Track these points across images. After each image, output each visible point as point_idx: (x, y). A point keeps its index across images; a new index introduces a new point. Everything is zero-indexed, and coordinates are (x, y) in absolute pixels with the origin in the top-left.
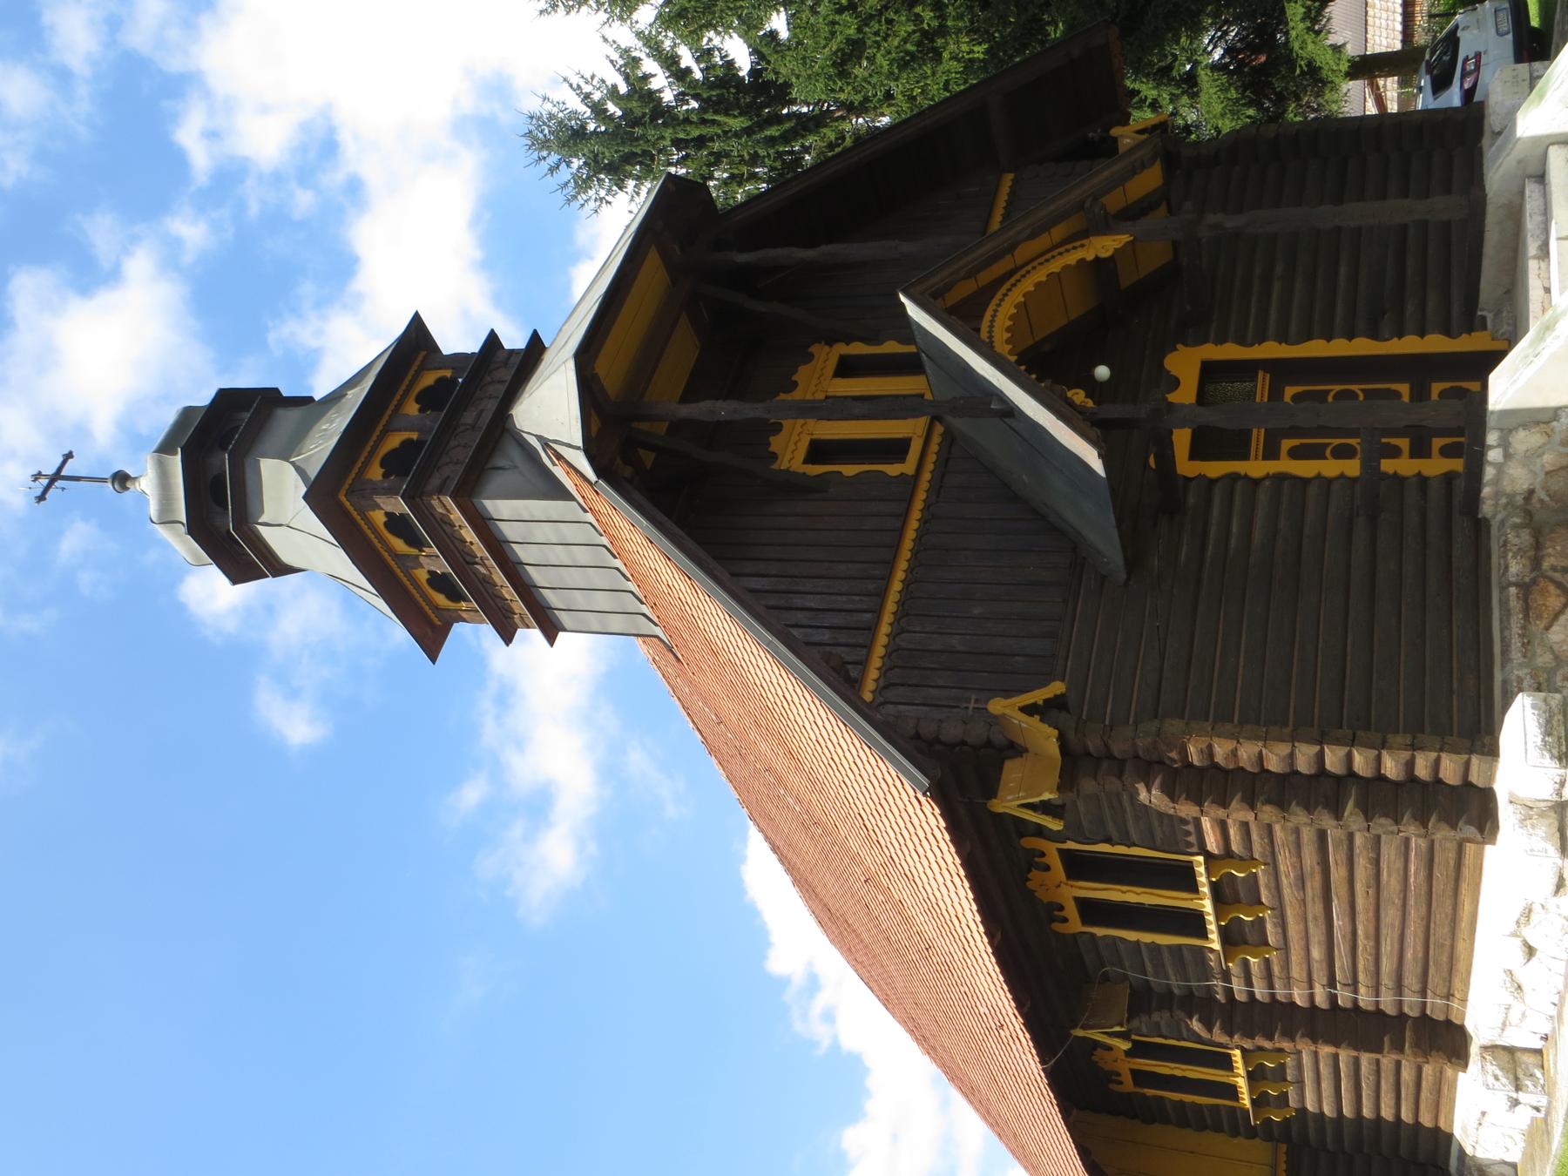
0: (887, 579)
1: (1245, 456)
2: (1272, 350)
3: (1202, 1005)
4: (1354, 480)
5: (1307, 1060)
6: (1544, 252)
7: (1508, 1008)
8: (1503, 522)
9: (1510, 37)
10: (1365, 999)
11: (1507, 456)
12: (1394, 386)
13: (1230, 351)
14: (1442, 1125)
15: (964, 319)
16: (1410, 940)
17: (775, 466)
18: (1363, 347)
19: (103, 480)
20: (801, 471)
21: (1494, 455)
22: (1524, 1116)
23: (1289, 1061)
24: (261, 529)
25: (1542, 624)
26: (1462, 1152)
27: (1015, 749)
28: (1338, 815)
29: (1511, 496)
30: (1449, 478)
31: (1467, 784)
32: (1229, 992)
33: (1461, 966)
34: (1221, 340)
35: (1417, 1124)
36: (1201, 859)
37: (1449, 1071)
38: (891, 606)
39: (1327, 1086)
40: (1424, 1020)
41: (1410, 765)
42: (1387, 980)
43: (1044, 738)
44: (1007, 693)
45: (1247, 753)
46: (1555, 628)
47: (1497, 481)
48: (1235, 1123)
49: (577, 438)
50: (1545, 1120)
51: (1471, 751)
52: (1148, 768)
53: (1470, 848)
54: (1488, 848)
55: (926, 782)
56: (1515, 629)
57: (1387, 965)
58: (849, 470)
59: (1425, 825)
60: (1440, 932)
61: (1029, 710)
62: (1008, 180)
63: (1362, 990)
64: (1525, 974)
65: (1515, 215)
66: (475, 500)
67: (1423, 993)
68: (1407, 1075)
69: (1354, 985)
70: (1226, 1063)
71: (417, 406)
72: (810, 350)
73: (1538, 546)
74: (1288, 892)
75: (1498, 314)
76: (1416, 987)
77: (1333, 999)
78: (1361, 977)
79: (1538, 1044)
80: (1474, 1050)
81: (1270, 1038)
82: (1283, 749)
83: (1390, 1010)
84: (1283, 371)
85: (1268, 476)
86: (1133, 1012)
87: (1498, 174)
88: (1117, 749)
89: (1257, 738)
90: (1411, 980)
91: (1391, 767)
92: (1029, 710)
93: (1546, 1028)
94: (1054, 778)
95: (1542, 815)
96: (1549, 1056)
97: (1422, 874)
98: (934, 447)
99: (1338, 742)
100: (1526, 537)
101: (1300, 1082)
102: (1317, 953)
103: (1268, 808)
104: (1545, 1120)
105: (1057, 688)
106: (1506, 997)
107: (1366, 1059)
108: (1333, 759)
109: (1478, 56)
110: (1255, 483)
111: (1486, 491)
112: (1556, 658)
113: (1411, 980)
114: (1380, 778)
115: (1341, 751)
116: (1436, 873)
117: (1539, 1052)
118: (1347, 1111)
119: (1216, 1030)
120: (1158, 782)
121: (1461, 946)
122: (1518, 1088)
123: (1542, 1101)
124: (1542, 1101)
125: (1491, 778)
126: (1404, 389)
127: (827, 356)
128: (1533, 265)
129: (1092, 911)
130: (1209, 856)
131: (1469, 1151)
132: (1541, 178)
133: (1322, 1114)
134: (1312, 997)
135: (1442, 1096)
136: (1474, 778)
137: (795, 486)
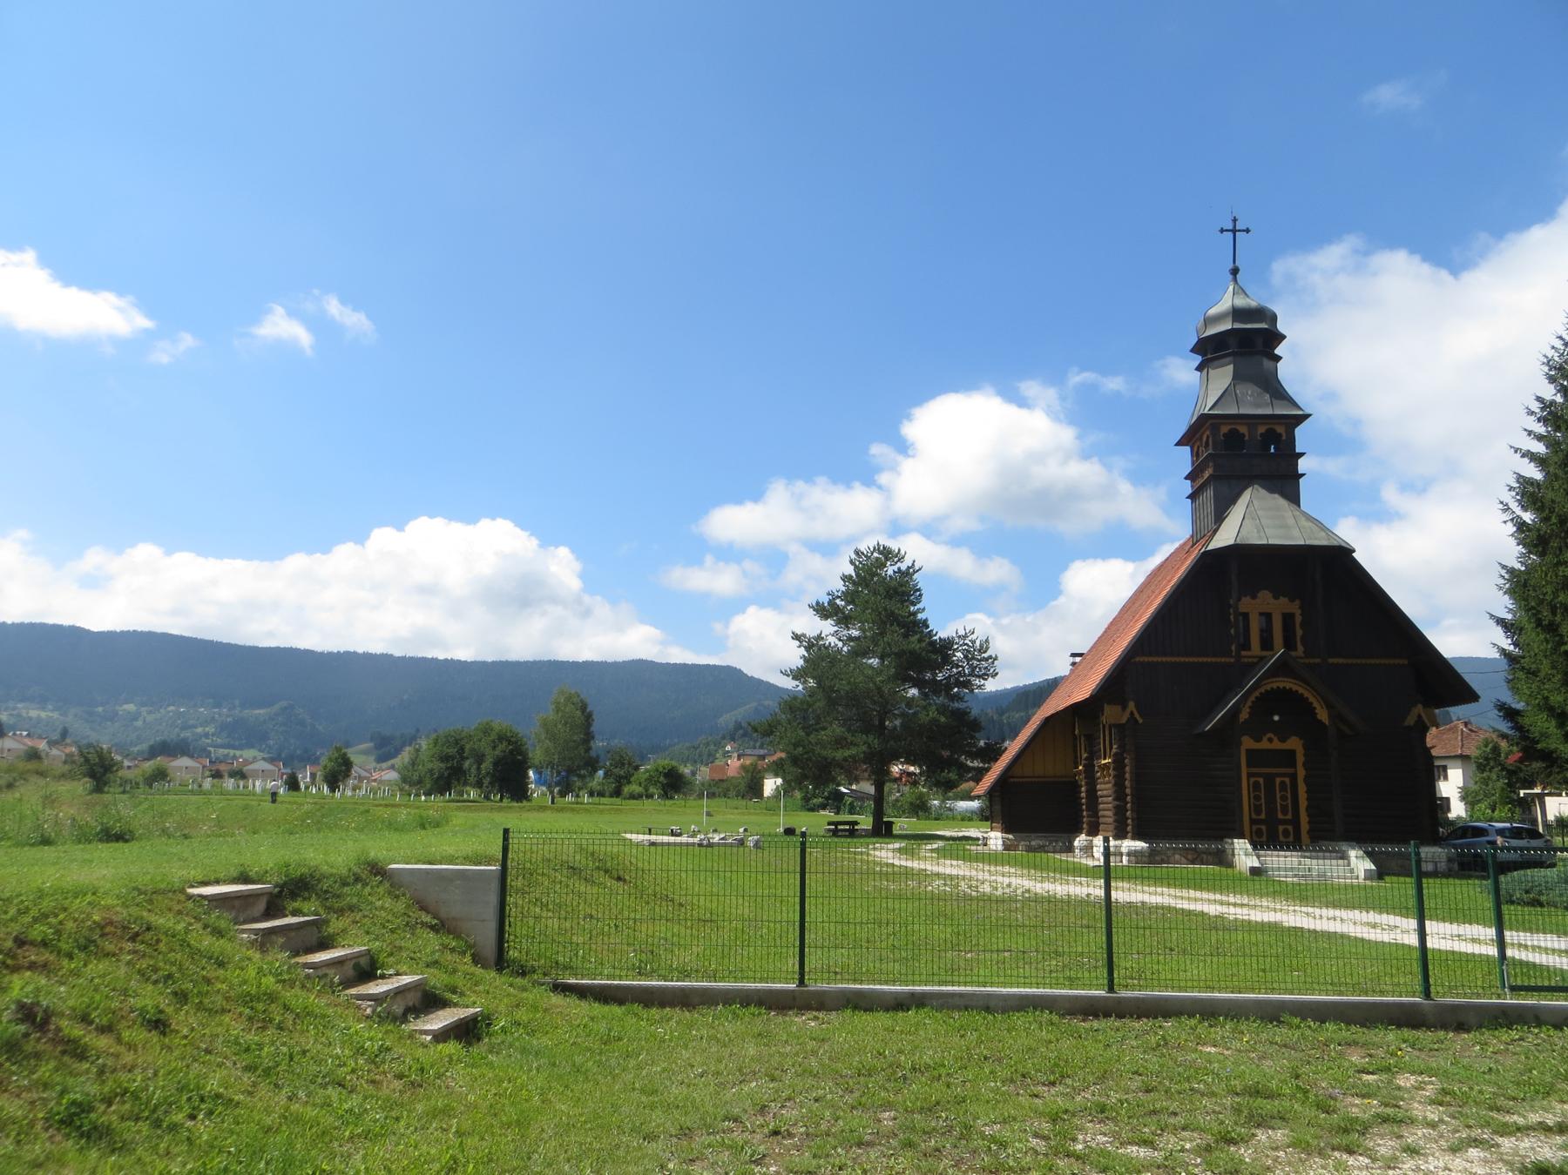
1: (1249, 766)
12: (1290, 813)
13: (1300, 759)
18: (1303, 803)
34: (1305, 755)
44: (1137, 707)
52: (1122, 747)
61: (1132, 713)
62: (1406, 662)
73: (1210, 854)
84: (1294, 777)
87: (1344, 846)
92: (1132, 713)
98: (1250, 660)
105: (1141, 721)
126: (1289, 817)
127: (1295, 608)
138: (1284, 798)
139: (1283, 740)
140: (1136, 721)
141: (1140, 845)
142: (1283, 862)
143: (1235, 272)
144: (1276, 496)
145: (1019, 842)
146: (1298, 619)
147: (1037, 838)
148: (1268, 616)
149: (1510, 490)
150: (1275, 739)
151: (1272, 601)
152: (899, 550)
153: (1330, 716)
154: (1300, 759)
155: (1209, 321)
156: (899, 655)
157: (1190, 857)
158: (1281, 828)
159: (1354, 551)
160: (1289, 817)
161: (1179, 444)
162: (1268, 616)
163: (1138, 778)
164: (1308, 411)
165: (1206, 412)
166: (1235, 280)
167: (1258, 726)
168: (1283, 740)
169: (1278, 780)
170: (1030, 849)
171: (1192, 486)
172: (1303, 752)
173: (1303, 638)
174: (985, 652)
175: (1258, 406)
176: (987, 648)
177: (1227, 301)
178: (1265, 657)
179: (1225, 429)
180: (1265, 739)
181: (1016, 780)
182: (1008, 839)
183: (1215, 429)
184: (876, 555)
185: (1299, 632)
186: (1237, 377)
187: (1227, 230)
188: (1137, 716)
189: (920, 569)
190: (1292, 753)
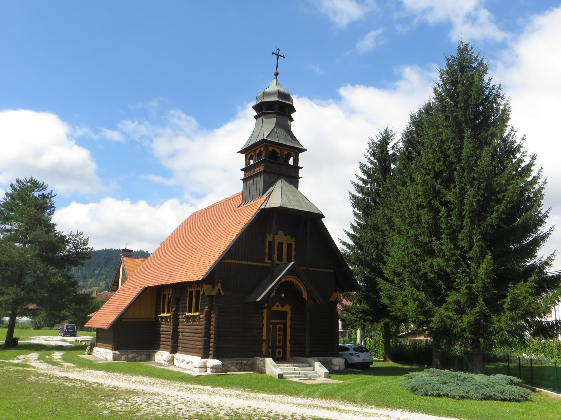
0: (244, 260)
2: (289, 323)
3: (177, 311)
4: (262, 337)
5: (170, 326)
6: (294, 366)
7: (180, 360)
8: (253, 360)
9: (362, 362)
10: (180, 337)
11: (261, 361)
12: (282, 343)
13: (289, 316)
14: (161, 349)
15: (291, 272)
16: (189, 345)
17: (268, 235)
18: (288, 337)
19: (277, 69)
20: (266, 240)
21: (261, 359)
22: (163, 362)
23: (169, 323)
24: (262, 117)
25: (235, 365)
26: (156, 352)
27: (213, 286)
28: (204, 337)
29: (256, 361)
30: (262, 352)
31: (209, 355)
32: (180, 315)
33: (186, 353)
34: (291, 314)
35: (160, 344)
36: (199, 314)
37: (170, 350)
38: (239, 262)
39: (166, 329)
40: (177, 347)
41: (212, 347)
42: (183, 341)
43: (214, 293)
45: (213, 323)
46: (234, 367)
47: (258, 359)
48: (158, 313)
49: (267, 207)
50: (163, 366)
51: (214, 355)
52: (211, 308)
53: (200, 355)
54: (200, 357)
55: (204, 278)
56: (234, 362)
57: (185, 341)
58: (267, 250)
59: (203, 349)
60: (190, 350)
61: (219, 290)
62: (332, 271)
63: (181, 337)
64: (184, 363)
65: (306, 362)
66: (263, 174)
67: (181, 347)
68: (169, 343)
69: (182, 336)
70: (168, 312)
71: (286, 154)
72: (294, 238)
73: (248, 365)
74: (195, 327)
75: (293, 359)
76: (182, 346)
77: (180, 332)
78: (183, 337)
79: (175, 364)
80: (173, 355)
81: (173, 322)
82: (213, 329)
83: (178, 341)
84: (285, 325)
85: (263, 323)
86: (175, 298)
87: (310, 360)
88: (213, 303)
89: (215, 325)
90: (183, 345)
91: (211, 344)
92: (219, 290)
93: (177, 366)
94: (208, 294)
95: (205, 365)
96: (173, 366)
97: (198, 348)
99: (215, 337)
100: (250, 363)
101: (166, 325)
102: (186, 330)
103: (205, 327)
104: (163, 366)
105: (223, 294)
106: (181, 360)
107: (170, 336)
108: (212, 336)
109: (359, 356)
110: (262, 321)
111: (257, 358)
112: (229, 367)
113: (183, 345)
114: (210, 343)
115: (213, 337)
116: (198, 350)
117: (173, 365)
118: (161, 332)
119: (173, 313)
120: (208, 310)
121: (189, 353)
122: (167, 361)
123: (166, 365)
124: (166, 365)
125: (210, 358)
126: (281, 344)
127: (292, 241)
128: (292, 365)
129: (191, 293)
130: (199, 315)
131: (156, 353)
132: (310, 366)
133: (161, 328)
134: (180, 329)
135: (165, 349)
136: (210, 356)
137: (264, 238)
138: (280, 335)
139: (283, 306)
140: (220, 294)
141: (218, 362)
142: (286, 369)
143: (277, 74)
144: (292, 186)
145: (122, 355)
146: (294, 247)
147: (132, 353)
148: (280, 244)
149: (350, 199)
150: (280, 305)
151: (284, 237)
152: (44, 183)
153: (308, 295)
154: (289, 316)
155: (265, 94)
156: (41, 243)
157: (239, 367)
158: (277, 350)
159: (323, 217)
160: (281, 344)
161: (240, 152)
162: (280, 244)
163: (218, 325)
164: (305, 147)
165: (265, 138)
166: (277, 78)
167: (277, 298)
168: (283, 306)
169: (278, 326)
170: (128, 360)
171: (245, 174)
172: (290, 312)
173: (295, 256)
174: (86, 245)
175: (286, 141)
176: (87, 244)
177: (273, 87)
178: (279, 264)
179: (271, 149)
180: (275, 305)
181: (125, 320)
182: (116, 354)
183: (266, 148)
184: (29, 184)
185: (293, 253)
186: (277, 125)
187: (275, 54)
188: (221, 291)
189: (55, 196)
190: (286, 312)
